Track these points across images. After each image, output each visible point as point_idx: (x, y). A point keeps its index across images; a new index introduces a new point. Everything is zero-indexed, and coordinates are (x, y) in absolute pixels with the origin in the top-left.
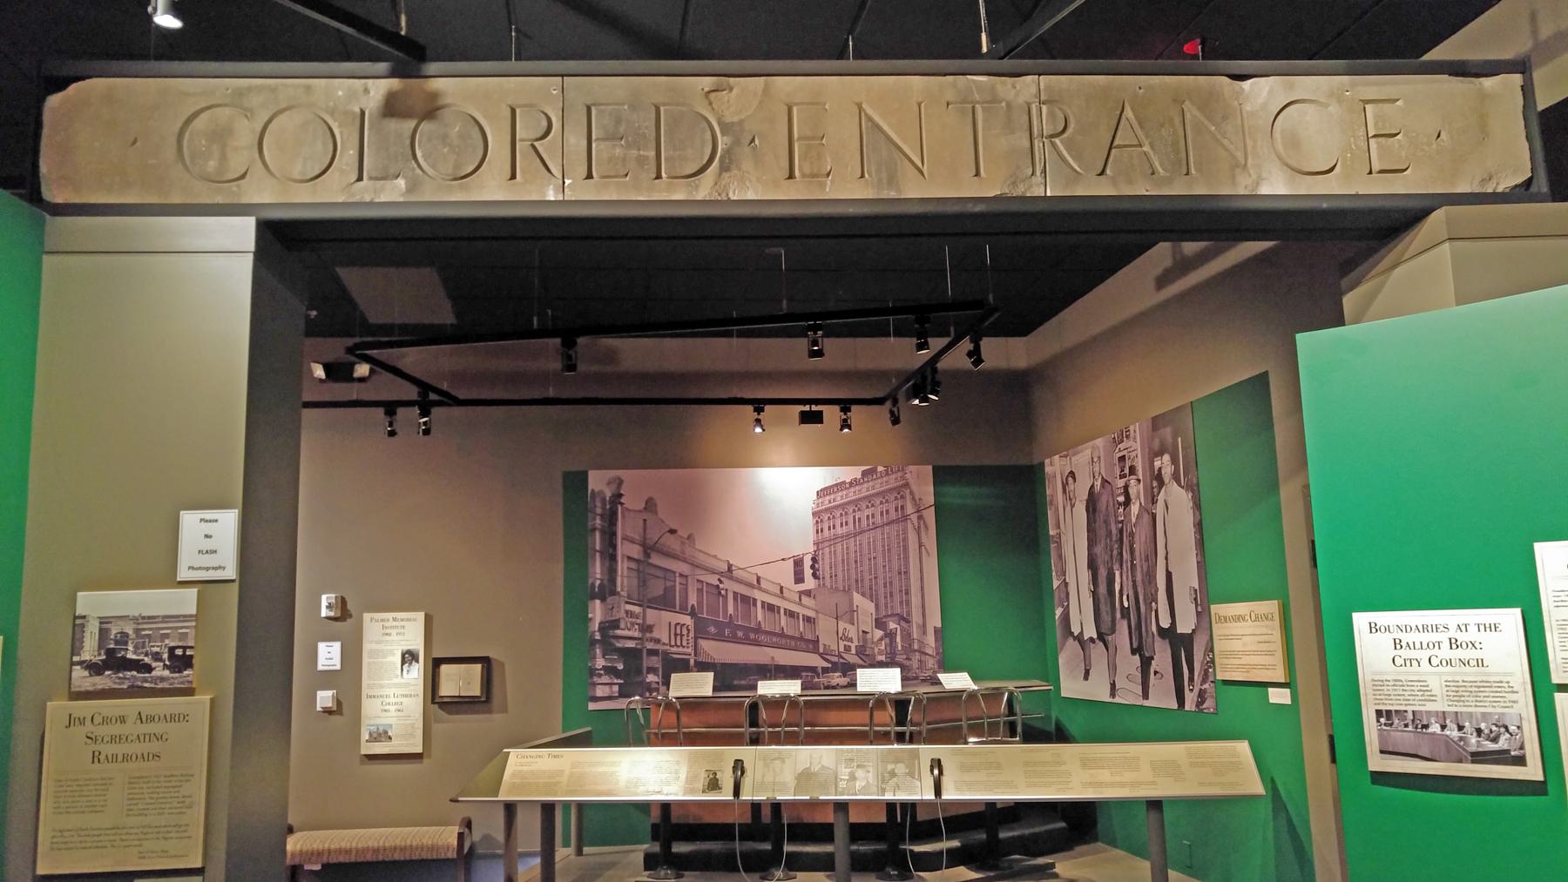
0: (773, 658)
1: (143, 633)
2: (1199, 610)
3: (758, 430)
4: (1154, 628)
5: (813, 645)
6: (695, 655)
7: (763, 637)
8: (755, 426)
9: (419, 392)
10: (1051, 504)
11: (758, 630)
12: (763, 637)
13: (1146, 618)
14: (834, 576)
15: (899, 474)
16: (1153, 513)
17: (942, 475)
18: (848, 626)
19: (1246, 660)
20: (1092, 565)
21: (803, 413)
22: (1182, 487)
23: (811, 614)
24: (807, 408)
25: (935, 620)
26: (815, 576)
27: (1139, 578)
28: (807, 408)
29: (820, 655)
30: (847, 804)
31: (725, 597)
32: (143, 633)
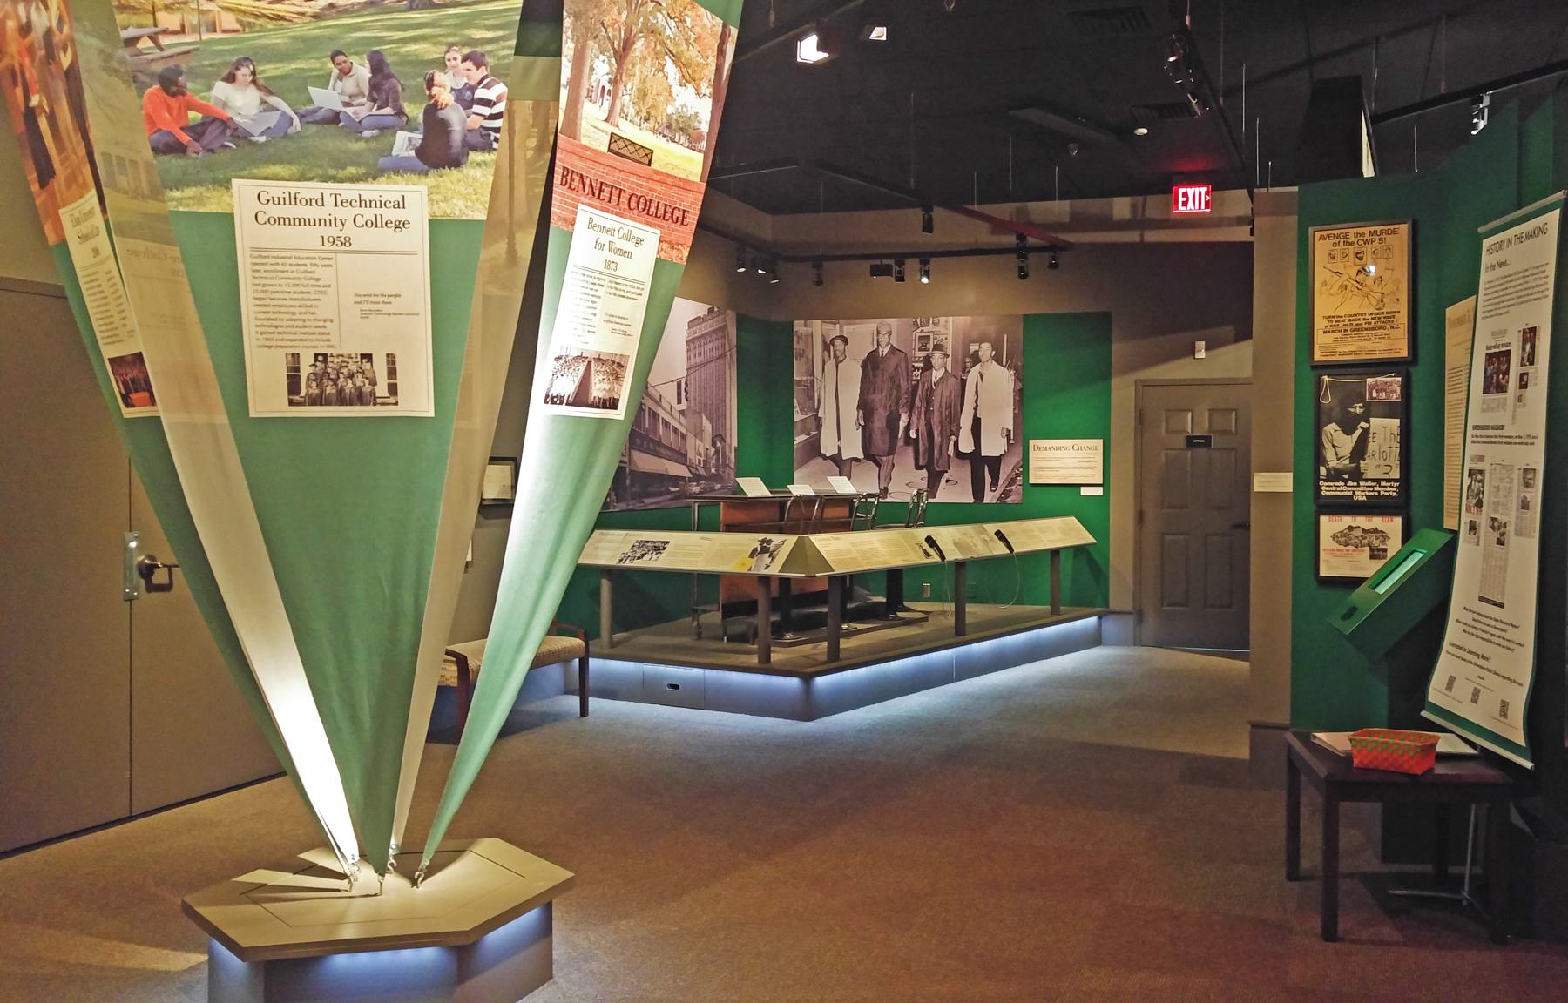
0: (666, 469)
1: (1195, 441)
2: (1012, 442)
3: (925, 280)
4: (951, 451)
5: (681, 457)
6: (630, 464)
7: (663, 451)
8: (921, 276)
9: (451, 127)
10: (801, 355)
11: (659, 443)
12: (663, 451)
13: (941, 446)
14: (695, 399)
15: (721, 317)
16: (962, 379)
17: (741, 322)
18: (701, 443)
19: (1062, 472)
20: (865, 406)
21: (873, 267)
22: (1005, 367)
23: (684, 431)
24: (878, 262)
25: (735, 444)
26: (687, 400)
27: (936, 419)
28: (878, 262)
29: (688, 466)
30: (769, 578)
31: (645, 411)
32: (1195, 441)
